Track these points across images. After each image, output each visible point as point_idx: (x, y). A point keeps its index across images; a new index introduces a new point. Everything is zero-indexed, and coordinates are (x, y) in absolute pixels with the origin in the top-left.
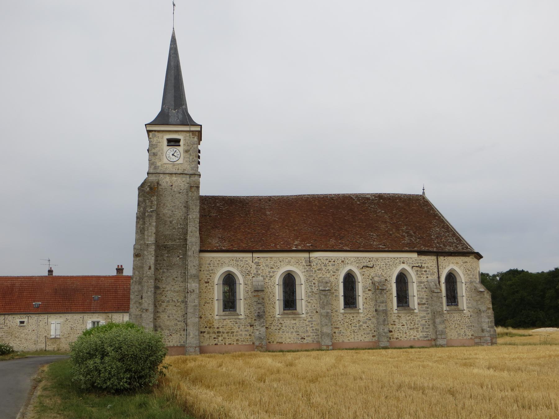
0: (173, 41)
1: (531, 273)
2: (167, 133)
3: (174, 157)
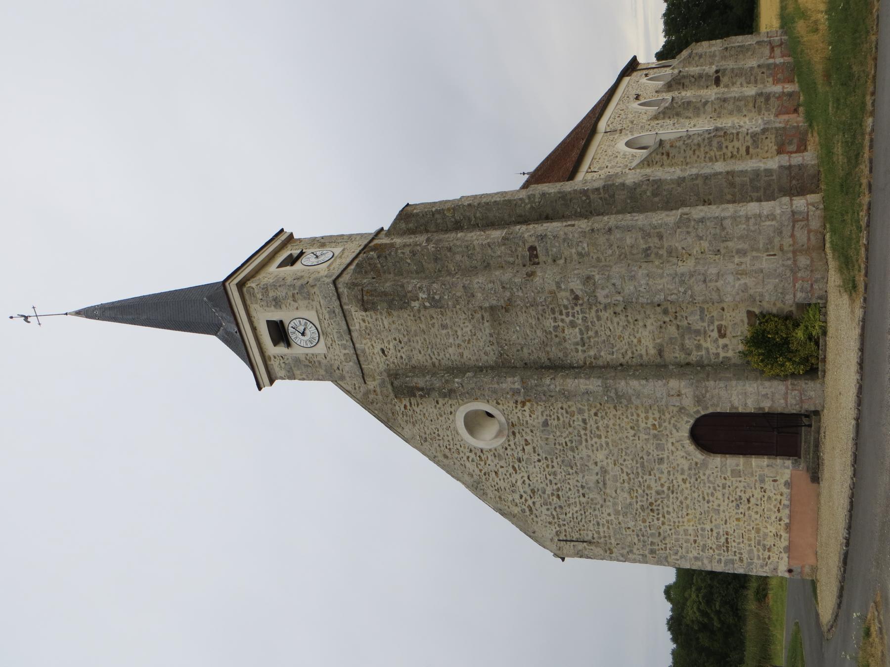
0: (89, 313)
1: (673, 659)
2: (264, 347)
3: (307, 332)
